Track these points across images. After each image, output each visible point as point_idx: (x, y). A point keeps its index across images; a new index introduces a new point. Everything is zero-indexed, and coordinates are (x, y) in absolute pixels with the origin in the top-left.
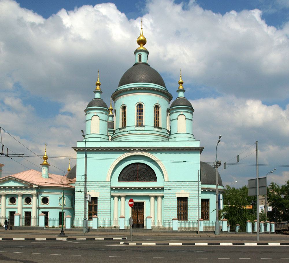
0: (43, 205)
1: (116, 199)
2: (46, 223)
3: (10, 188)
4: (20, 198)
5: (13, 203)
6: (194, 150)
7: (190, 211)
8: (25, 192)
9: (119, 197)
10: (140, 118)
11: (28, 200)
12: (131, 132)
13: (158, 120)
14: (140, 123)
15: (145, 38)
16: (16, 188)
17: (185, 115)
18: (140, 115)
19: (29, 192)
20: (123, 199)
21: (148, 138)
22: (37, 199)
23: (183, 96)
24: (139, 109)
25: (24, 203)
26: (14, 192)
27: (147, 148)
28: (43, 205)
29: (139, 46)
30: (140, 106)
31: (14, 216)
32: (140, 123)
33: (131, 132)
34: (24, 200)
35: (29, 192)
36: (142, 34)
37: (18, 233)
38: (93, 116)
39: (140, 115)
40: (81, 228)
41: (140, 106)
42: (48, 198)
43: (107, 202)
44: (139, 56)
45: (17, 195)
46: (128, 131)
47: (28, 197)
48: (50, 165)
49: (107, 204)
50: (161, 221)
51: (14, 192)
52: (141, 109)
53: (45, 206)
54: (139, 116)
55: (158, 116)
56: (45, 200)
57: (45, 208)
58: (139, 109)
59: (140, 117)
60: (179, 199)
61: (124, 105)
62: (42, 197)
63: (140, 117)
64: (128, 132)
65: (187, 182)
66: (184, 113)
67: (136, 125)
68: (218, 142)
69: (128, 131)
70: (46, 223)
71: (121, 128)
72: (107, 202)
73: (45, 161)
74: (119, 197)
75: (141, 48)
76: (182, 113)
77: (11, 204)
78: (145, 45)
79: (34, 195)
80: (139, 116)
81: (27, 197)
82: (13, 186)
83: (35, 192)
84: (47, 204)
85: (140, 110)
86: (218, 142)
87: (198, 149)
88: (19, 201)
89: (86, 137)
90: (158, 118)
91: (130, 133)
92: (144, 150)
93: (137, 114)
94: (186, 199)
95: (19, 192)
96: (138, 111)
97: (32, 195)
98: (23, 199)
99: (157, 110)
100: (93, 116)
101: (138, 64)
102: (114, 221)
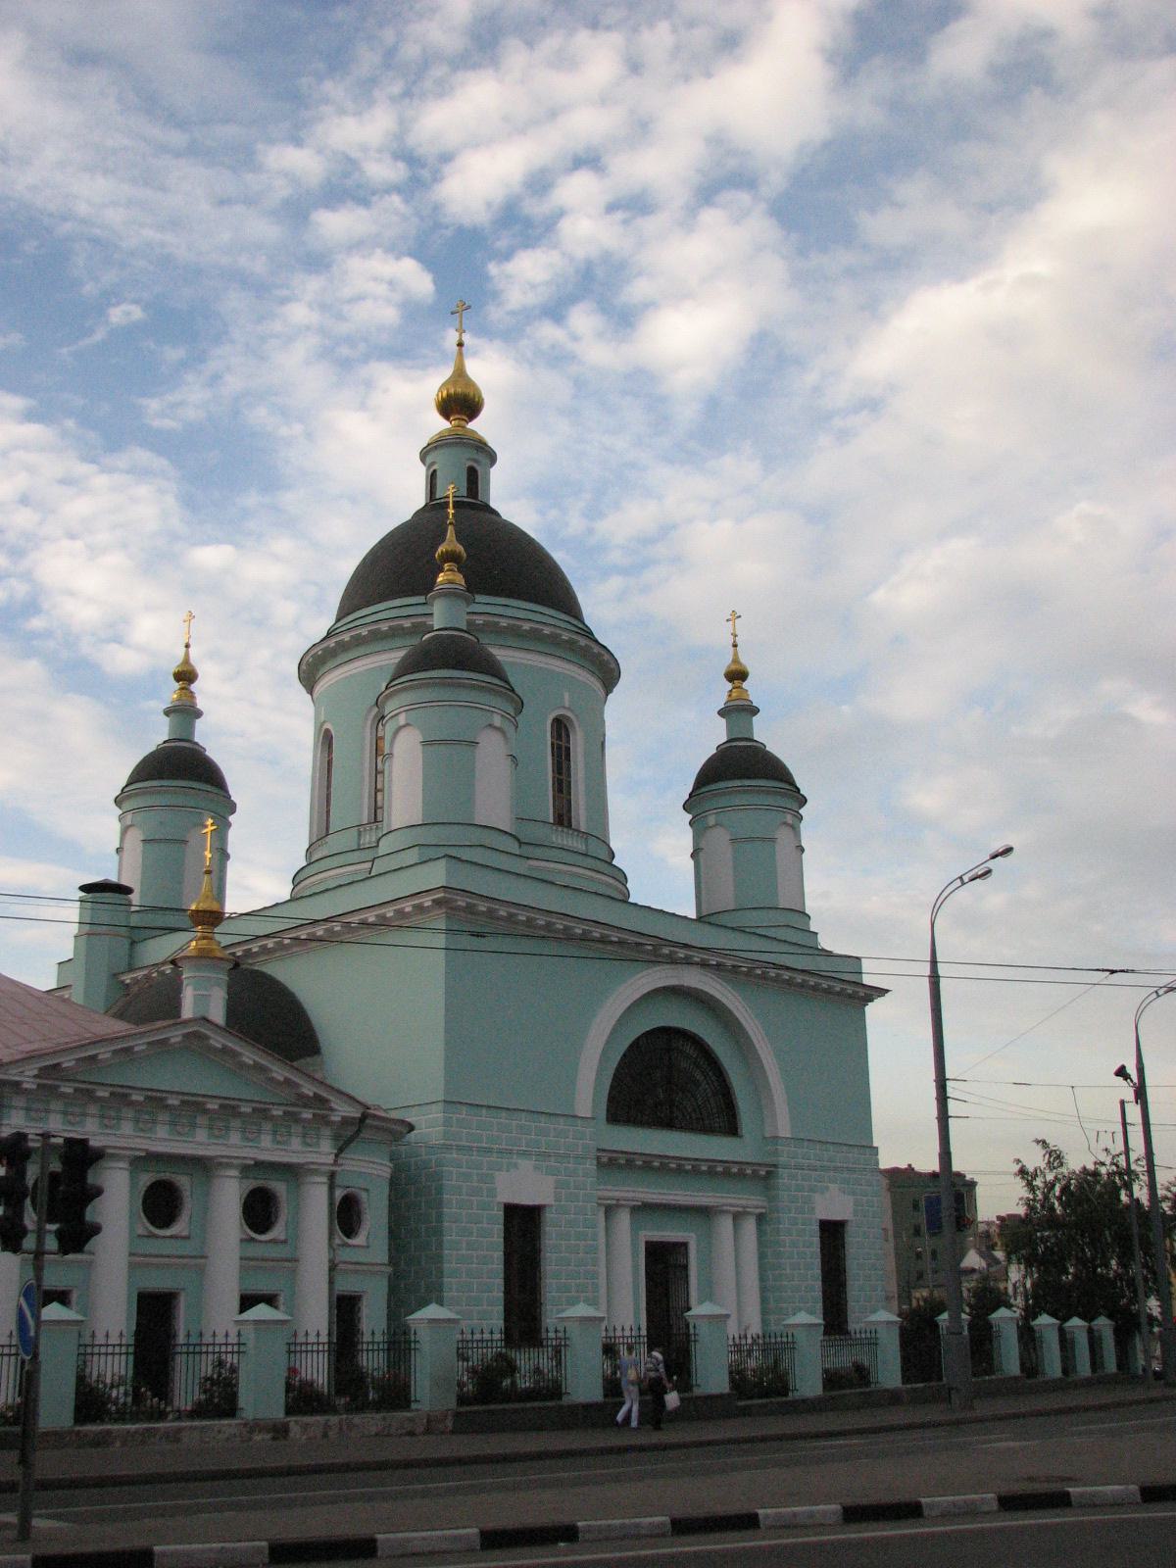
26: (199, 1143)
42: (363, 1196)
99: (563, 744)
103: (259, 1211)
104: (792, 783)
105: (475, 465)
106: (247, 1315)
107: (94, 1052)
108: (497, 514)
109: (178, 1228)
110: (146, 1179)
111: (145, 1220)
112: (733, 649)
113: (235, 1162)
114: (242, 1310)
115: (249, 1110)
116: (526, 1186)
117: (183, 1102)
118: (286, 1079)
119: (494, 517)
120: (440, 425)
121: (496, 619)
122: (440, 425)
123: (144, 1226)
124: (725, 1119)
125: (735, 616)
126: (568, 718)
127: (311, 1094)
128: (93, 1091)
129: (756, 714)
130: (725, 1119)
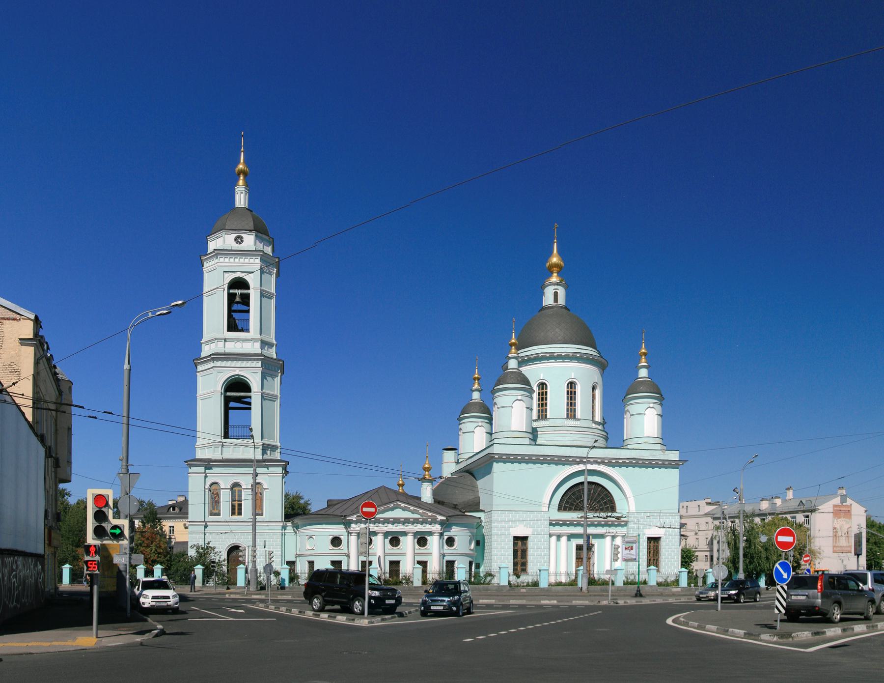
0: (392, 549)
1: (554, 538)
3: (396, 521)
5: (395, 547)
9: (559, 537)
10: (571, 405)
11: (422, 541)
13: (575, 406)
14: (571, 413)
16: (406, 521)
18: (571, 399)
22: (440, 538)
23: (647, 376)
24: (570, 390)
25: (388, 546)
26: (400, 528)
28: (392, 549)
31: (62, 569)
32: (571, 413)
34: (387, 541)
35: (428, 528)
37: (522, 597)
38: (515, 401)
39: (571, 399)
44: (555, 292)
45: (405, 534)
51: (400, 528)
52: (573, 390)
55: (575, 399)
56: (450, 541)
58: (570, 390)
59: (571, 403)
60: (516, 538)
63: (571, 403)
68: (17, 382)
73: (427, 473)
79: (380, 533)
80: (570, 401)
82: (391, 518)
84: (339, 548)
85: (571, 392)
86: (17, 382)
88: (408, 543)
89: (494, 436)
90: (575, 403)
92: (602, 462)
94: (524, 539)
95: (410, 528)
97: (430, 533)
98: (414, 538)
99: (573, 390)
100: (515, 401)
101: (552, 307)
102: (560, 574)
106: (649, 568)
113: (437, 532)
116: (654, 532)
130: (613, 509)
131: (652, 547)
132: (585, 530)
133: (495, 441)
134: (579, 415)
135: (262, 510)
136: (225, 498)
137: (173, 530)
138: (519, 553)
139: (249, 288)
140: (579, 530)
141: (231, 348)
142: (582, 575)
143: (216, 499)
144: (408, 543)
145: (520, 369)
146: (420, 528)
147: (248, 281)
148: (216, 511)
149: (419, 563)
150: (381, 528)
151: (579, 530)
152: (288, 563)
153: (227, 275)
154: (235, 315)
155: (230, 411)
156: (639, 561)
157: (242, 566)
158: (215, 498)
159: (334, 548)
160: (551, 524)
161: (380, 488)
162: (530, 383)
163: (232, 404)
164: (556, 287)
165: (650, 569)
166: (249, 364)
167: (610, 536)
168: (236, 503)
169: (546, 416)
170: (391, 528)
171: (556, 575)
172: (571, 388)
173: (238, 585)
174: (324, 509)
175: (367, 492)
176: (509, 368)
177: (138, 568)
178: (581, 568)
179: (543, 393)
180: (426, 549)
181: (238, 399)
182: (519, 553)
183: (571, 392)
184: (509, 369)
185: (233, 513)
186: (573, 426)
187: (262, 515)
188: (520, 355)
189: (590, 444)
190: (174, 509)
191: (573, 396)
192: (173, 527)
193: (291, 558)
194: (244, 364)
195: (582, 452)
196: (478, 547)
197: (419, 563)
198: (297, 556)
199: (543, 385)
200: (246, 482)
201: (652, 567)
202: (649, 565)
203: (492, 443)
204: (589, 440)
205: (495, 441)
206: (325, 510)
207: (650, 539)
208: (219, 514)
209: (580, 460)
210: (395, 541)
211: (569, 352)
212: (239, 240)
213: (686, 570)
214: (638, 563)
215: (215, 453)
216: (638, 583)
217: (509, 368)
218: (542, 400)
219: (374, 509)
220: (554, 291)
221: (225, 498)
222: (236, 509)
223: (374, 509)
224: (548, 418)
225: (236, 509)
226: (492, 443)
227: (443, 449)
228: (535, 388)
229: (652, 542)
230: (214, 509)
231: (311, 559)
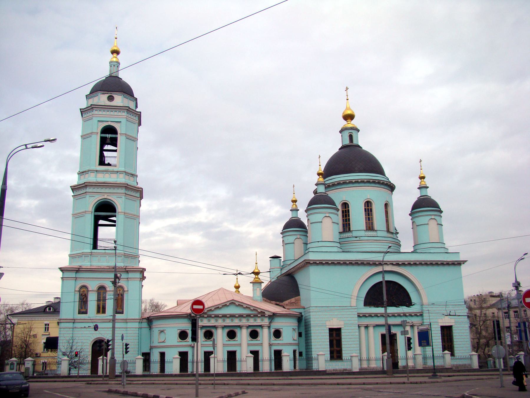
1: (363, 329)
2: (162, 368)
3: (232, 316)
4: (220, 331)
6: (341, 264)
7: (458, 343)
8: (252, 322)
9: (367, 327)
11: (254, 335)
12: (362, 238)
14: (370, 227)
15: (353, 112)
16: (241, 316)
17: (331, 217)
19: (259, 322)
20: (371, 329)
21: (373, 246)
24: (367, 208)
26: (236, 322)
27: (408, 261)
29: (345, 122)
30: (368, 204)
32: (370, 227)
33: (362, 238)
35: (259, 322)
36: (348, 106)
40: (440, 367)
41: (368, 204)
42: (281, 330)
43: (354, 334)
46: (356, 237)
47: (254, 329)
48: (263, 283)
49: (354, 337)
50: (368, 358)
52: (369, 208)
53: (278, 341)
54: (370, 217)
56: (277, 334)
57: (278, 344)
60: (331, 330)
61: (388, 203)
62: (180, 330)
63: (369, 218)
64: (358, 239)
65: (451, 306)
66: (331, 215)
67: (365, 229)
69: (356, 237)
70: (162, 368)
71: (342, 232)
72: (354, 334)
74: (367, 327)
75: (350, 126)
76: (433, 217)
77: (229, 341)
78: (354, 120)
79: (244, 327)
81: (253, 329)
83: (266, 321)
84: (185, 340)
85: (368, 209)
87: (316, 262)
88: (243, 335)
89: (309, 246)
91: (360, 239)
92: (398, 264)
93: (366, 215)
94: (339, 330)
95: (244, 322)
96: (365, 209)
97: (261, 326)
103: (254, 335)
104: (439, 207)
105: (352, 134)
106: (444, 352)
107: (211, 309)
108: (361, 147)
109: (259, 338)
110: (250, 330)
111: (274, 337)
112: (348, 95)
113: (245, 326)
114: (443, 352)
115: (238, 316)
116: (447, 321)
117: (239, 316)
118: (254, 309)
119: (360, 149)
120: (344, 123)
121: (358, 180)
122: (344, 123)
123: (250, 338)
124: (408, 303)
125: (421, 161)
126: (388, 204)
127: (260, 311)
128: (211, 316)
129: (296, 202)
130: (408, 303)
131: (445, 334)
132: (386, 320)
133: (310, 250)
134: (376, 227)
135: (123, 309)
136: (92, 299)
137: (48, 328)
138: (335, 342)
139: (117, 134)
140: (382, 321)
141: (101, 178)
142: (386, 359)
143: (85, 300)
144: (243, 335)
145: (327, 193)
146: (252, 322)
147: (102, 128)
148: (84, 310)
149: (252, 352)
150: (220, 322)
151: (382, 321)
152: (144, 354)
153: (100, 123)
154: (106, 153)
155: (99, 227)
156: (432, 346)
157: (30, 358)
158: (83, 298)
159: (182, 341)
160: (359, 316)
161: (220, 289)
162: (335, 203)
163: (101, 222)
164: (350, 131)
165: (445, 354)
166: (116, 191)
167: (364, 326)
168: (101, 303)
169: (349, 228)
170: (228, 322)
171: (369, 360)
172: (368, 206)
173: (99, 374)
174: (174, 307)
175: (210, 293)
176: (318, 192)
177: (99, 359)
178: (386, 354)
179: (346, 211)
180: (186, 341)
181: (106, 218)
182: (335, 342)
183: (368, 209)
184: (318, 193)
185: (98, 312)
186: (371, 236)
187: (122, 313)
188: (326, 182)
189: (385, 250)
190: (50, 309)
191: (347, 214)
192: (48, 325)
193: (146, 350)
194: (112, 190)
195: (378, 257)
196: (300, 338)
197: (252, 352)
198: (151, 348)
199: (345, 205)
200: (93, 286)
201: (446, 352)
202: (444, 349)
203: (307, 252)
204: (384, 247)
205: (310, 250)
206: (175, 308)
207: (443, 328)
208: (86, 313)
209: (380, 264)
210: (232, 335)
211: (364, 179)
212: (111, 98)
213: (476, 354)
214: (431, 347)
215: (85, 262)
216: (197, 375)
217: (318, 192)
218: (346, 217)
219: (202, 306)
220: (350, 134)
221: (92, 299)
222: (101, 309)
223: (202, 306)
224: (351, 230)
225: (101, 309)
226: (307, 252)
227: (270, 258)
228: (340, 207)
229: (445, 330)
230: (82, 308)
231: (162, 350)
